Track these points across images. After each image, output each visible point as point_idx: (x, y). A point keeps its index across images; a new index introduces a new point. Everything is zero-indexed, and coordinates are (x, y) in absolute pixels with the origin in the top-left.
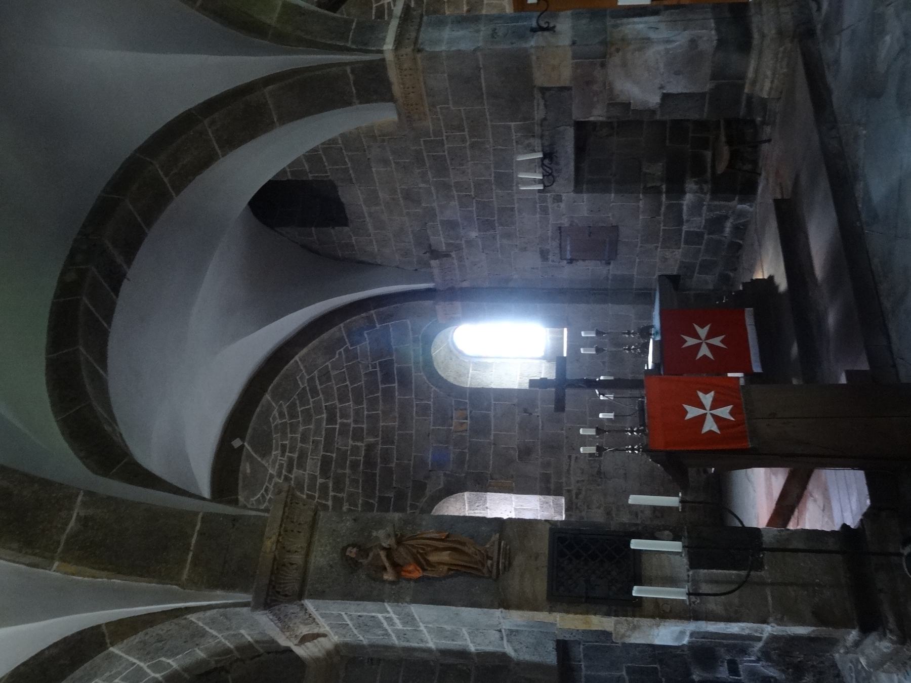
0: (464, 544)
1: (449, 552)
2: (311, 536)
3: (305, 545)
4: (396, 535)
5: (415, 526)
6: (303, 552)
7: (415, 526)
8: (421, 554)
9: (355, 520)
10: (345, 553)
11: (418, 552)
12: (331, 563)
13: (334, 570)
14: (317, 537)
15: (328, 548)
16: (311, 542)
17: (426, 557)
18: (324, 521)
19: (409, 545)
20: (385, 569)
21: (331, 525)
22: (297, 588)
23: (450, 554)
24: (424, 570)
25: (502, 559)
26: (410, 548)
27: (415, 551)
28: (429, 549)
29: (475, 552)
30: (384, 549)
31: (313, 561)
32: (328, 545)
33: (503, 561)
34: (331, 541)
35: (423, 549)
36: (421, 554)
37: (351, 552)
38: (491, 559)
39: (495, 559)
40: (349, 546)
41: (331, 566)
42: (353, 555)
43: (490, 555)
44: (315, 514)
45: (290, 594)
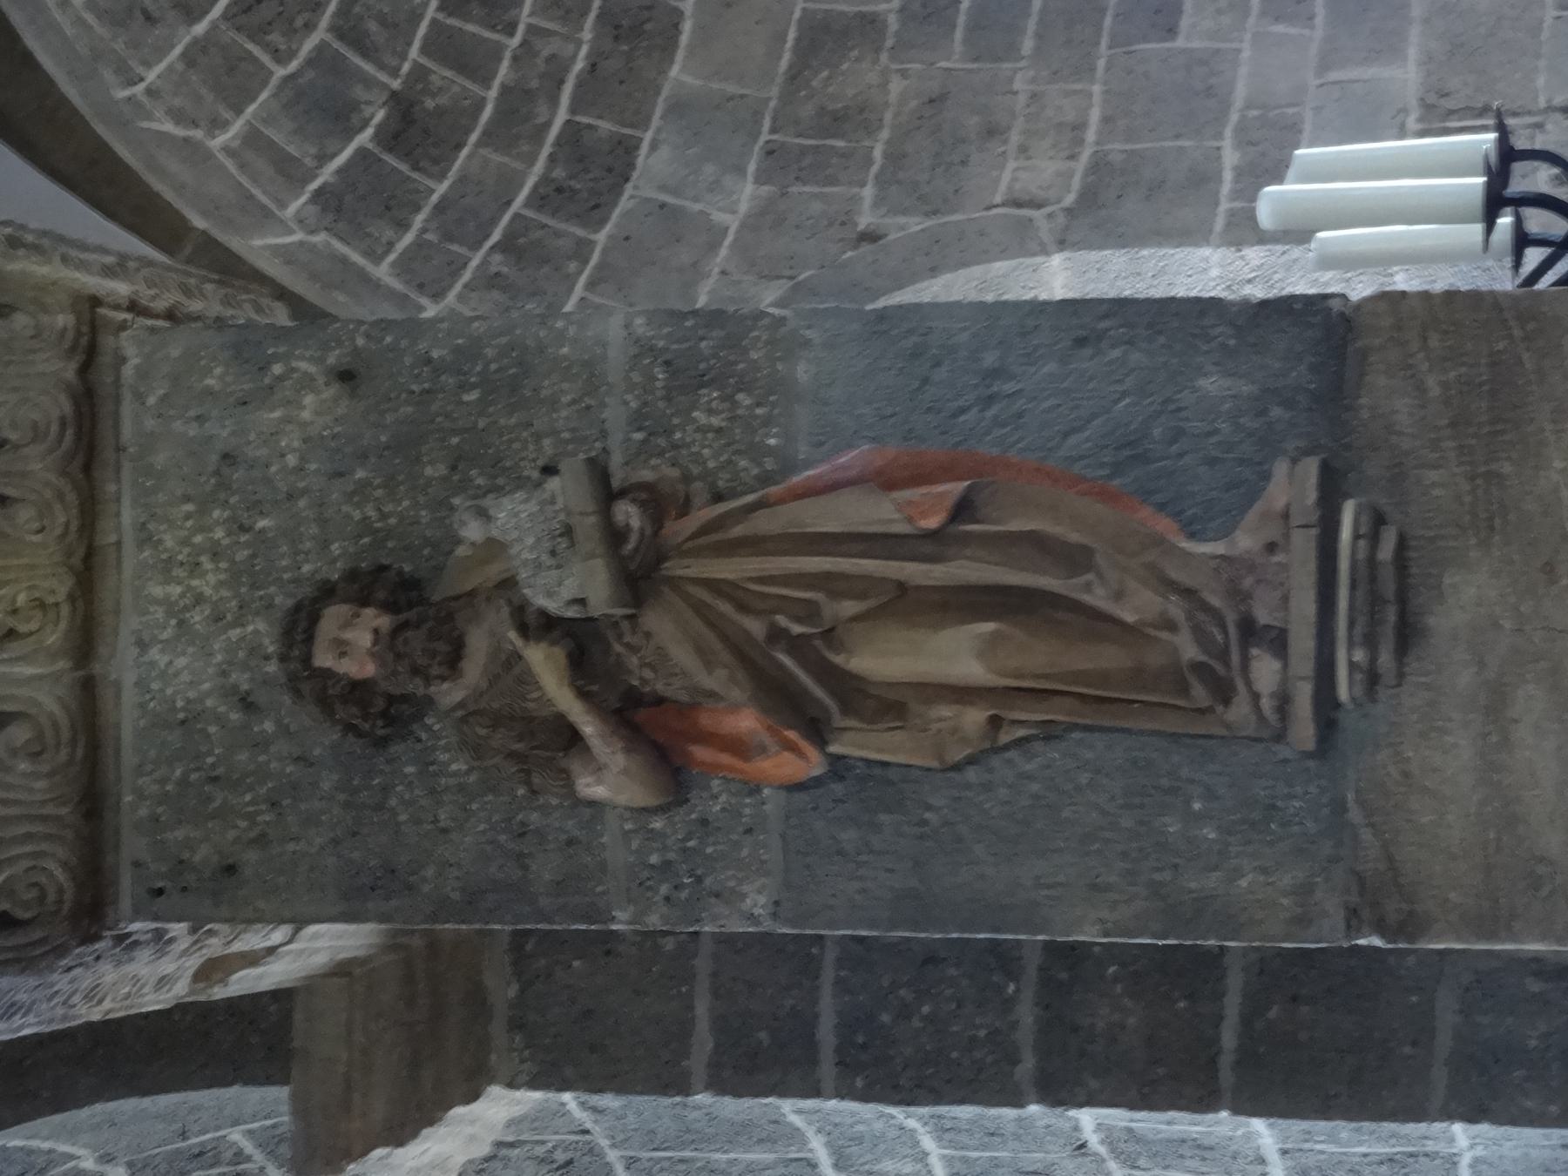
0: (1075, 559)
1: (989, 626)
2: (90, 509)
3: (60, 587)
4: (615, 536)
5: (744, 399)
6: (53, 638)
7: (744, 399)
8: (797, 646)
9: (346, 376)
10: (307, 660)
11: (777, 635)
12: (242, 680)
13: (269, 726)
14: (128, 516)
15: (208, 582)
16: (90, 553)
17: (838, 659)
18: (151, 400)
19: (709, 584)
20: (572, 739)
21: (200, 419)
22: (60, 874)
23: (994, 640)
24: (817, 730)
25: (1351, 645)
26: (725, 607)
27: (756, 627)
28: (850, 607)
29: (1186, 265)
30: (544, 626)
31: (129, 678)
32: (207, 564)
33: (1359, 656)
34: (219, 533)
35: (809, 612)
36: (797, 646)
37: (342, 648)
38: (1279, 643)
39: (1303, 642)
40: (327, 593)
41: (247, 704)
42: (360, 667)
43: (1263, 616)
44: (85, 369)
45: (27, 915)
